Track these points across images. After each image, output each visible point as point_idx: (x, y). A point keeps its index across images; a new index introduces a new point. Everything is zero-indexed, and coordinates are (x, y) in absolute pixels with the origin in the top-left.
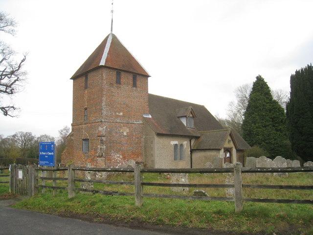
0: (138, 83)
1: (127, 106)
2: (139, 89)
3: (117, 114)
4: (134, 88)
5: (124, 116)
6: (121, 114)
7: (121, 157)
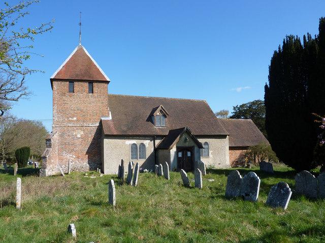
0: (95, 89)
1: (82, 111)
2: (96, 95)
3: (70, 119)
4: (91, 94)
5: (78, 120)
6: (75, 119)
7: (74, 157)
